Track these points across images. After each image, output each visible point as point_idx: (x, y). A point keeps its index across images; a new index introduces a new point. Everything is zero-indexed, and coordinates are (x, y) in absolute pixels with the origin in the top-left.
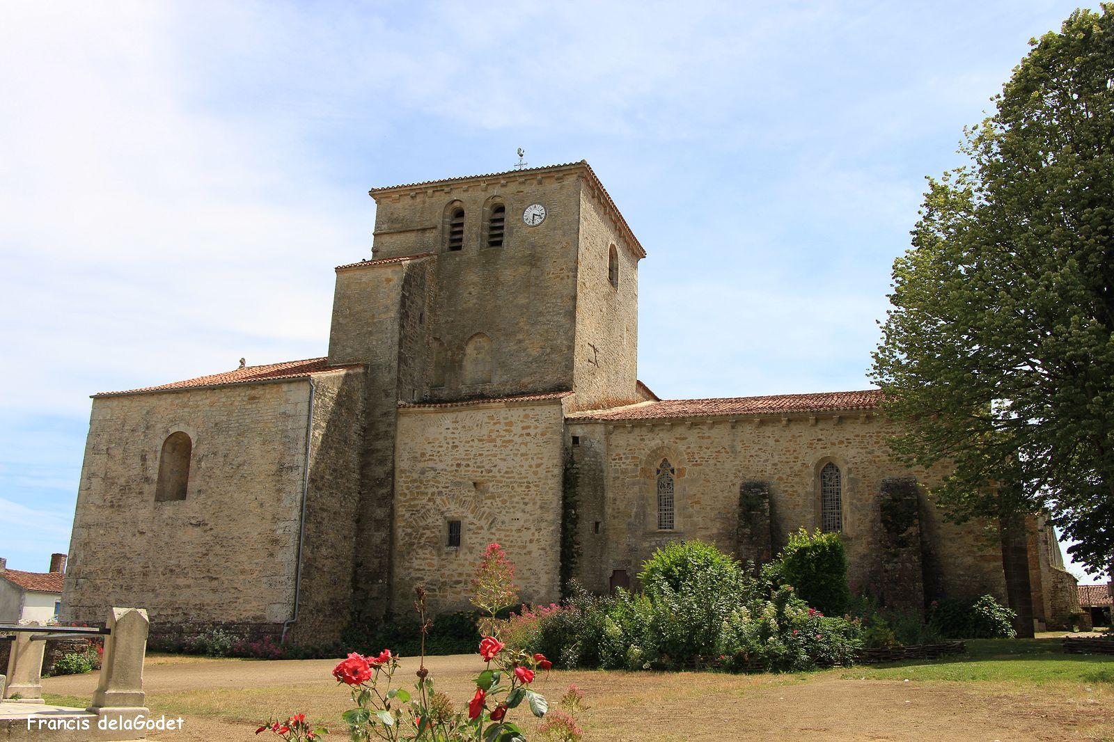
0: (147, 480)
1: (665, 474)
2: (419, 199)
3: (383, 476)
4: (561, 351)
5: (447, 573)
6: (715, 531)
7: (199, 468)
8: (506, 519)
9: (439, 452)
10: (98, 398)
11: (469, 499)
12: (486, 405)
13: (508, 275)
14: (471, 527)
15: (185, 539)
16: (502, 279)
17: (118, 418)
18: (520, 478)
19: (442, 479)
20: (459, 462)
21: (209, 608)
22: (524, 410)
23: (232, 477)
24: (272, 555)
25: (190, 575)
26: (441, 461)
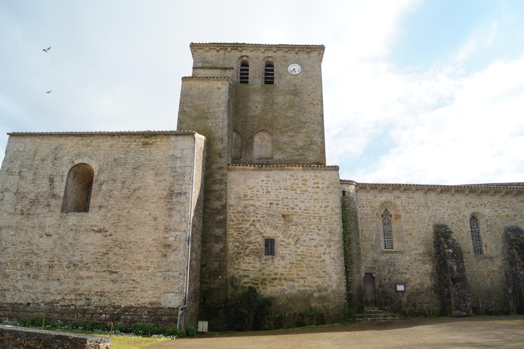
0: (54, 196)
1: (386, 216)
2: (222, 52)
3: (219, 208)
4: (317, 144)
5: (266, 273)
6: (421, 251)
7: (100, 190)
8: (307, 239)
9: (257, 195)
10: (12, 135)
11: (279, 225)
12: (290, 167)
13: (280, 99)
14: (282, 243)
15: (87, 241)
16: (276, 101)
17: (30, 150)
18: (314, 214)
19: (260, 212)
20: (271, 202)
21: (109, 295)
22: (314, 173)
23: (129, 198)
24: (165, 256)
25: (92, 269)
26: (258, 200)
